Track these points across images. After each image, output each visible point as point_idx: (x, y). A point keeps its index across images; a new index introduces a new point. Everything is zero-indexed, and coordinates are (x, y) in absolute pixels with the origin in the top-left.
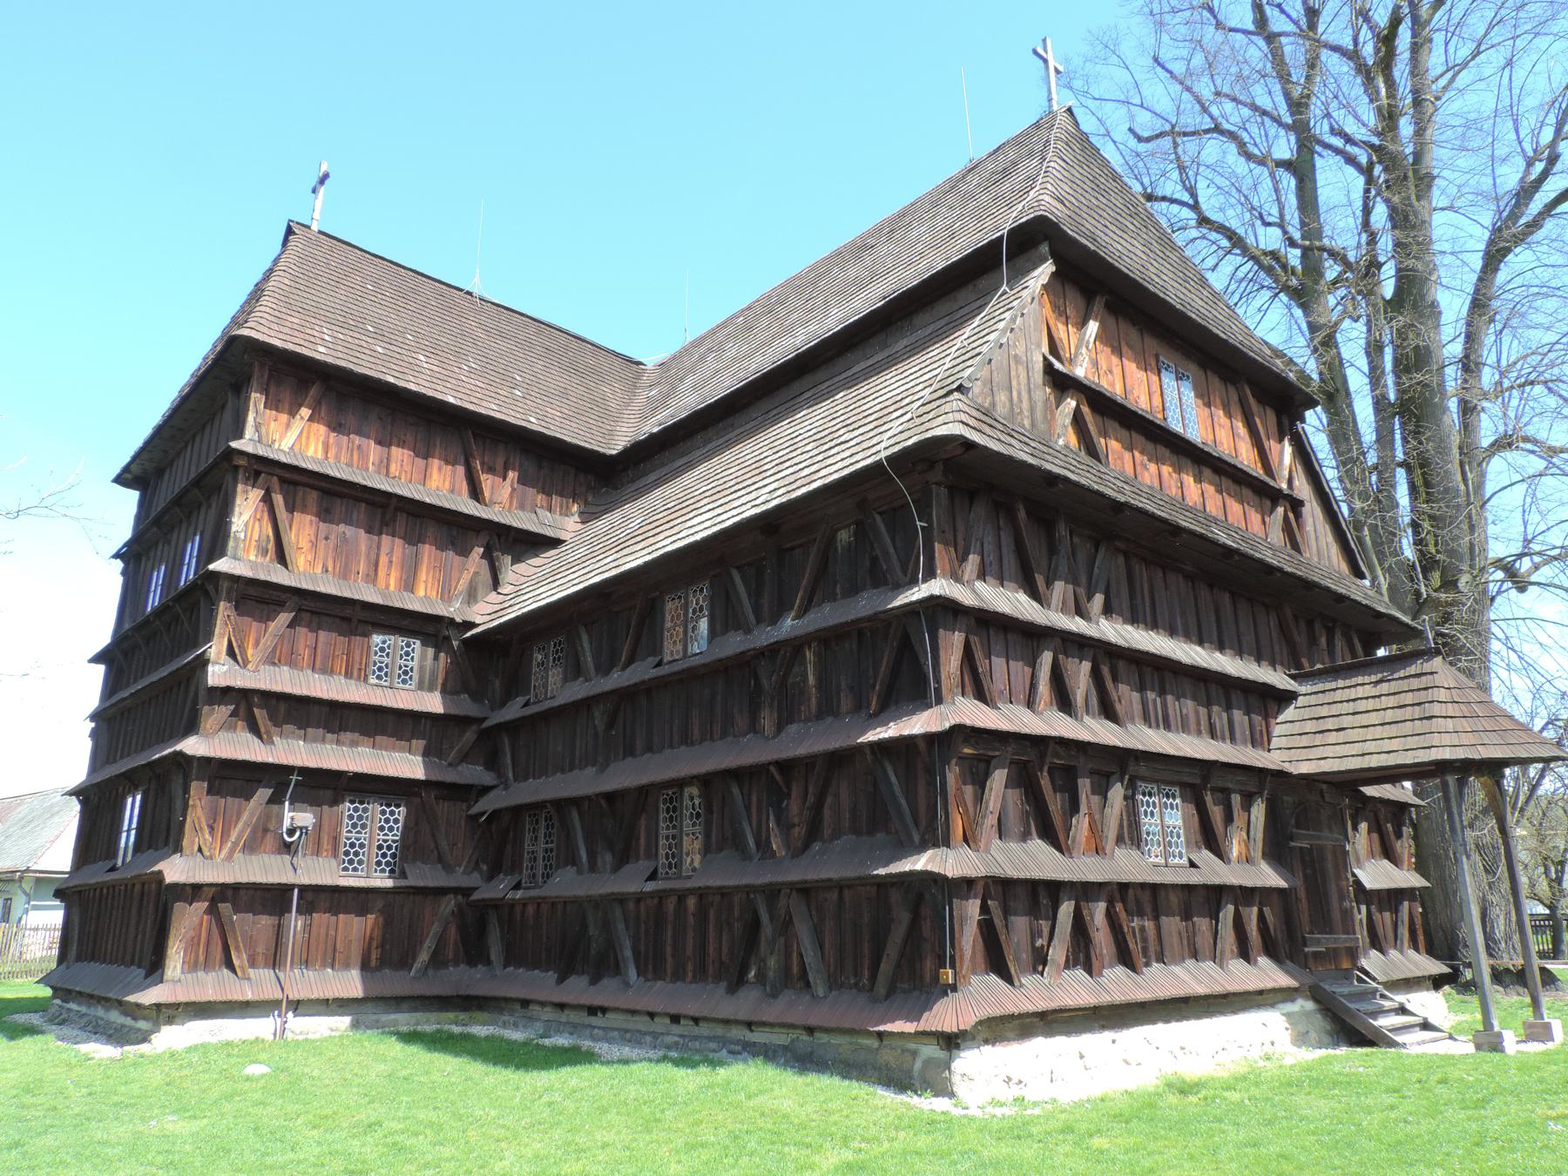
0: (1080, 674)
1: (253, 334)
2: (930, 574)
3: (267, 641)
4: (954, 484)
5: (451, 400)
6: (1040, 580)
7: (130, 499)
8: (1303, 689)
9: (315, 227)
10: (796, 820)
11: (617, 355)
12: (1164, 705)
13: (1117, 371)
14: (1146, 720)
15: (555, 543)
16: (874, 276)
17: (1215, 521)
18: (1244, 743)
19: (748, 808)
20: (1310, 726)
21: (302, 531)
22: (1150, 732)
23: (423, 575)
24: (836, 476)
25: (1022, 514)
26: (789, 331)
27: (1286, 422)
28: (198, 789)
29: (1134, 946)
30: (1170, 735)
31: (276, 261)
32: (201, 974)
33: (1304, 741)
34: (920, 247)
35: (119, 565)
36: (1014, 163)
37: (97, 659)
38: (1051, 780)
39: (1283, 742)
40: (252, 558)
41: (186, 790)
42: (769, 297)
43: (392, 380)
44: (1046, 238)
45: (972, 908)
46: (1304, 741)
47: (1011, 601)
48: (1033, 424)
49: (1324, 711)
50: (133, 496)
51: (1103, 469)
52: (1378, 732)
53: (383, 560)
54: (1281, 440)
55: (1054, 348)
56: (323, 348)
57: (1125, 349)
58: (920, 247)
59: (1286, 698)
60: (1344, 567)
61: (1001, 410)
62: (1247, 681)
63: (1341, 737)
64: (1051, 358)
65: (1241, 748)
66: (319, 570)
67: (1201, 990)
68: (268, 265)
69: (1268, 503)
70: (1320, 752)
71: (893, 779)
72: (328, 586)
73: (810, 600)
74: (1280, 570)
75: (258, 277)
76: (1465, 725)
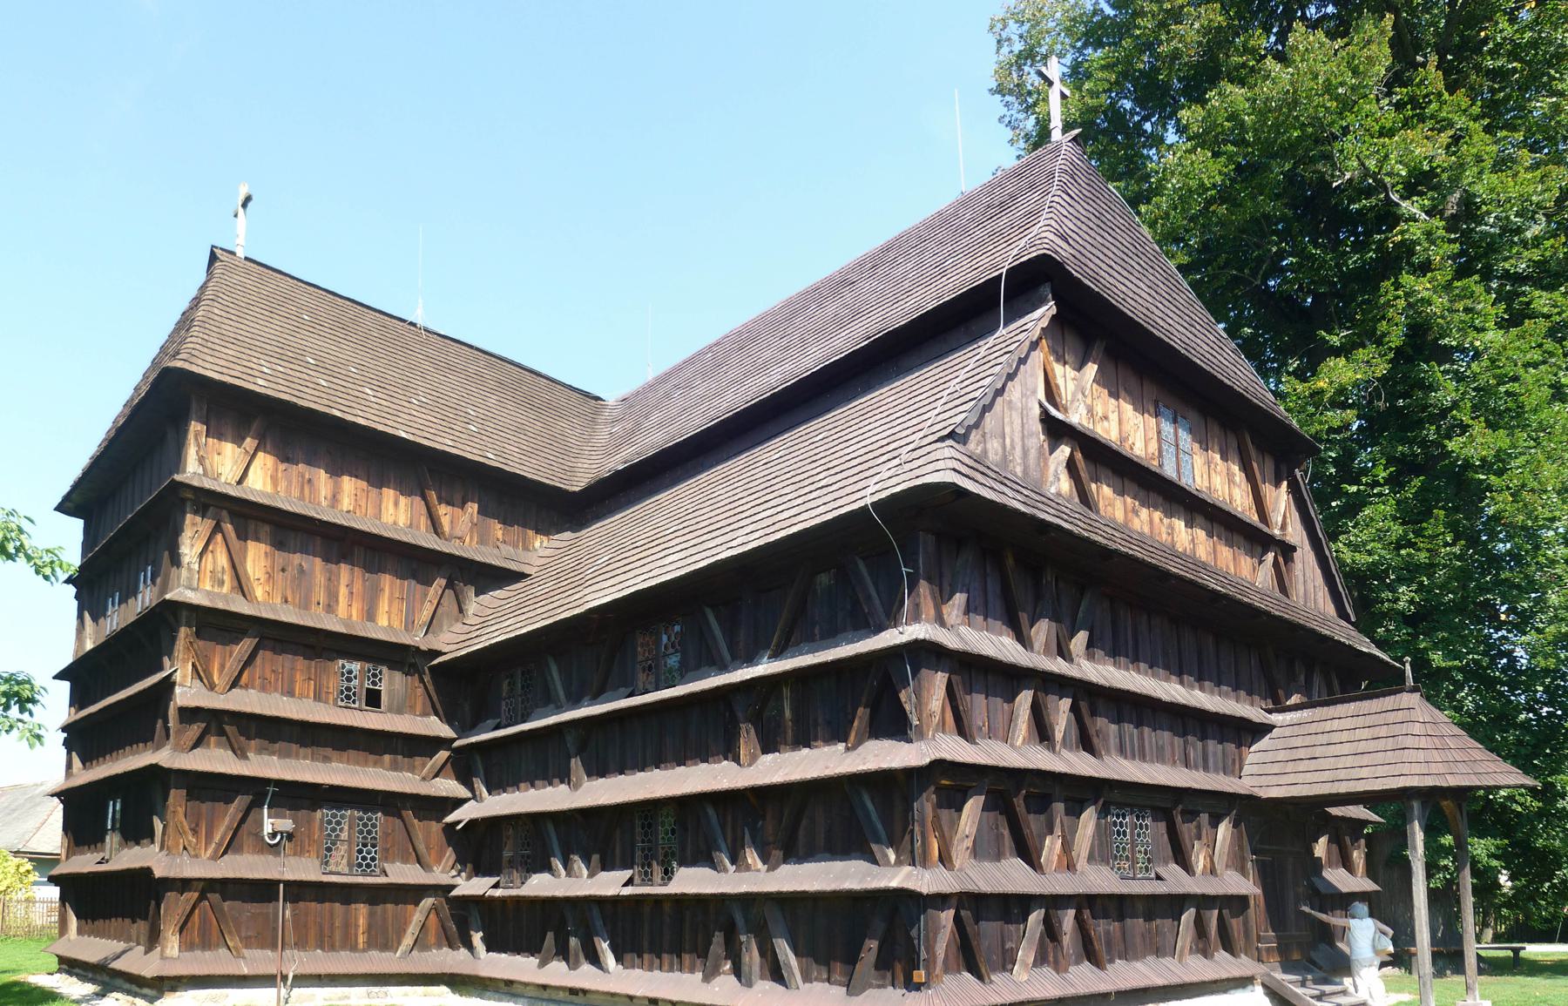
0: (1061, 712)
1: (186, 366)
2: (916, 617)
3: (233, 665)
4: (945, 532)
5: (404, 435)
6: (1024, 618)
7: (76, 525)
8: (1276, 718)
9: (241, 253)
10: (771, 839)
11: (570, 387)
12: (1141, 738)
13: (1114, 417)
14: (1122, 751)
15: (519, 576)
16: (856, 314)
17: (1204, 566)
18: (1216, 771)
19: (723, 827)
20: (1282, 756)
21: (257, 557)
22: (1125, 762)
23: (384, 605)
24: (818, 521)
25: (1010, 562)
26: (764, 368)
27: (1284, 468)
28: (176, 797)
29: (1100, 947)
30: (1145, 765)
31: (203, 288)
32: (198, 953)
33: (1276, 768)
34: (907, 284)
35: (72, 590)
36: (1013, 197)
37: (60, 676)
38: (1021, 803)
39: (1255, 769)
40: (208, 588)
41: (166, 799)
42: (740, 333)
43: (338, 414)
44: (1048, 279)
45: (947, 917)
46: (1276, 768)
47: (998, 644)
48: (1025, 472)
49: (1298, 742)
50: (78, 524)
51: (1094, 516)
52: (1349, 761)
53: (343, 591)
54: (1277, 485)
55: (1051, 392)
56: (262, 377)
57: (1122, 393)
58: (907, 284)
59: (1266, 729)
60: (1331, 610)
61: (993, 456)
62: (1224, 715)
63: (1313, 765)
64: (1047, 405)
65: (1212, 775)
66: (278, 600)
67: (1160, 982)
68: (194, 293)
69: (1259, 550)
70: (1291, 779)
71: (870, 806)
72: (289, 616)
73: (788, 640)
74: (1268, 614)
75: (185, 305)
76: (1436, 756)
